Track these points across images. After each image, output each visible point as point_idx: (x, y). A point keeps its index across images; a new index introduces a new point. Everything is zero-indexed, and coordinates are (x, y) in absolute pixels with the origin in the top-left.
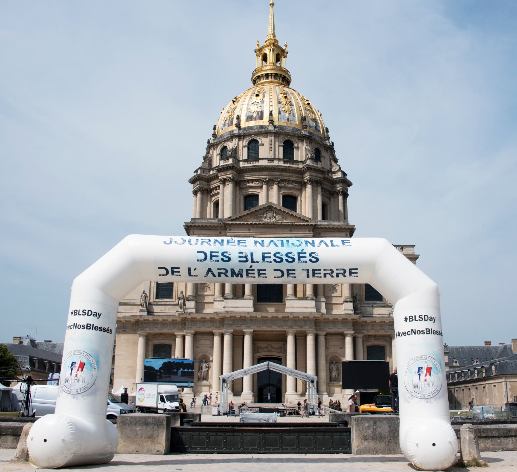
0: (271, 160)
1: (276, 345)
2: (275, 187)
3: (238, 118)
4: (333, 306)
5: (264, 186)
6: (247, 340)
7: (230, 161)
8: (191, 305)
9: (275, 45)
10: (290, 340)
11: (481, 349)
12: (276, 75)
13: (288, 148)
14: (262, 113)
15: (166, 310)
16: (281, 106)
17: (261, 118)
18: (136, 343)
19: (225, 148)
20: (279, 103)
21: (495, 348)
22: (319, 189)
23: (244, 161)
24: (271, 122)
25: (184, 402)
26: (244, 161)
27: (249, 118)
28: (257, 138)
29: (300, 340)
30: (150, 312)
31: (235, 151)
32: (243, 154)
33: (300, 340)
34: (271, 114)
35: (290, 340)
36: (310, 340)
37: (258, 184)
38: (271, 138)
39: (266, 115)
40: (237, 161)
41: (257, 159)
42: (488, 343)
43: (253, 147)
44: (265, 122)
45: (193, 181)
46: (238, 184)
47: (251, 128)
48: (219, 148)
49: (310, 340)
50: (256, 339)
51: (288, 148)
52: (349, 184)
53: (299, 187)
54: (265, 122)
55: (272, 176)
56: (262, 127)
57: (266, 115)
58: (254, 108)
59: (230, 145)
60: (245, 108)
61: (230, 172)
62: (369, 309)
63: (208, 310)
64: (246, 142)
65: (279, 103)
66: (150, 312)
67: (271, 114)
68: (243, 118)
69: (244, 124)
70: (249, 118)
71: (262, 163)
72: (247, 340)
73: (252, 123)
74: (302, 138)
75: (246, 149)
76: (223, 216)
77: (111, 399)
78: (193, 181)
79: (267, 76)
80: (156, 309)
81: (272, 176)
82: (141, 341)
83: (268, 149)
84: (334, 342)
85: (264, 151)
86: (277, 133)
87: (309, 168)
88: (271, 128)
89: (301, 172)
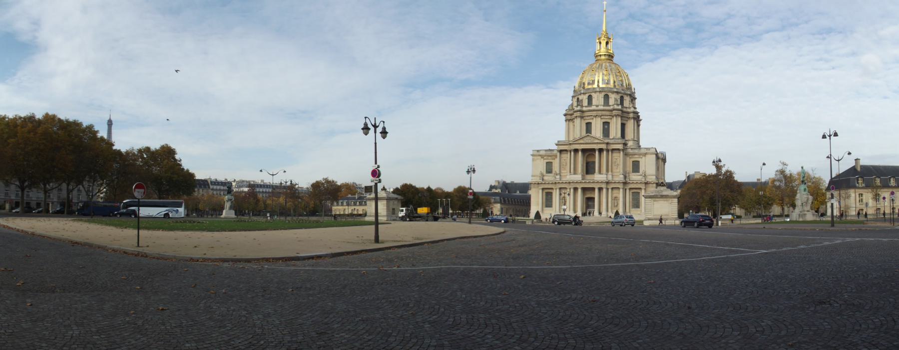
0: (597, 106)
7: (620, 107)
8: (558, 177)
10: (597, 191)
13: (606, 97)
15: (549, 178)
27: (589, 84)
29: (600, 189)
32: (585, 103)
33: (600, 189)
35: (597, 191)
36: (604, 190)
44: (595, 86)
45: (565, 115)
49: (604, 190)
51: (606, 97)
55: (598, 114)
62: (329, 203)
70: (589, 84)
71: (593, 108)
72: (580, 191)
73: (590, 87)
77: (400, 205)
78: (565, 115)
80: (545, 178)
81: (598, 114)
83: (598, 100)
84: (615, 191)
85: (594, 102)
86: (602, 90)
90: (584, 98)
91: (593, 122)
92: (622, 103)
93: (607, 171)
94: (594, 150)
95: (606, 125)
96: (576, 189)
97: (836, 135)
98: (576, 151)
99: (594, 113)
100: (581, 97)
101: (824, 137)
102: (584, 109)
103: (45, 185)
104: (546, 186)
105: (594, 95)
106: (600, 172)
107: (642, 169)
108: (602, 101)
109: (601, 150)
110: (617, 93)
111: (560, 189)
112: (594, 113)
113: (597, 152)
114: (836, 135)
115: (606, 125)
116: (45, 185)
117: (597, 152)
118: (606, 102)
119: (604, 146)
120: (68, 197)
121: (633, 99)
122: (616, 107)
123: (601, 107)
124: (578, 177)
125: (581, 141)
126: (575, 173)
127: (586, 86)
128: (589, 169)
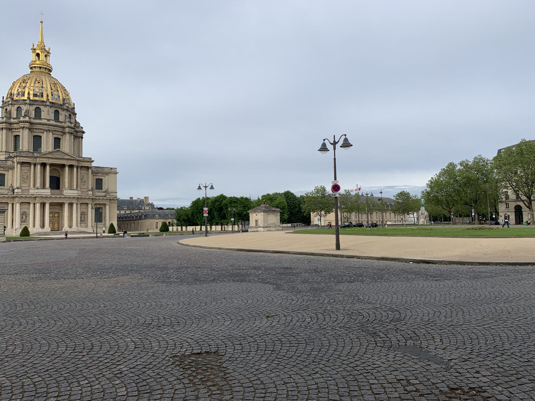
2: (51, 133)
4: (334, 236)
5: (45, 133)
6: (47, 206)
9: (43, 49)
11: (128, 200)
21: (135, 201)
22: (72, 136)
23: (14, 118)
24: (29, 98)
26: (14, 118)
29: (71, 205)
31: (10, 111)
32: (14, 114)
33: (71, 205)
37: (42, 131)
41: (40, 118)
42: (131, 198)
43: (38, 111)
44: (45, 99)
49: (75, 206)
53: (62, 134)
54: (26, 97)
56: (43, 102)
61: (4, 124)
64: (34, 107)
69: (15, 98)
72: (47, 206)
73: (37, 98)
75: (15, 112)
76: (23, 148)
78: (84, 132)
83: (47, 114)
85: (44, 115)
86: (32, 103)
90: (14, 110)
91: (44, 136)
92: (57, 119)
94: (63, 166)
96: (43, 205)
97: (346, 144)
98: (44, 165)
99: (45, 127)
100: (9, 108)
101: (324, 148)
106: (71, 188)
107: (104, 188)
108: (52, 116)
109: (71, 167)
112: (45, 127)
113: (67, 168)
114: (346, 144)
117: (67, 168)
118: (57, 119)
121: (72, 113)
125: (50, 156)
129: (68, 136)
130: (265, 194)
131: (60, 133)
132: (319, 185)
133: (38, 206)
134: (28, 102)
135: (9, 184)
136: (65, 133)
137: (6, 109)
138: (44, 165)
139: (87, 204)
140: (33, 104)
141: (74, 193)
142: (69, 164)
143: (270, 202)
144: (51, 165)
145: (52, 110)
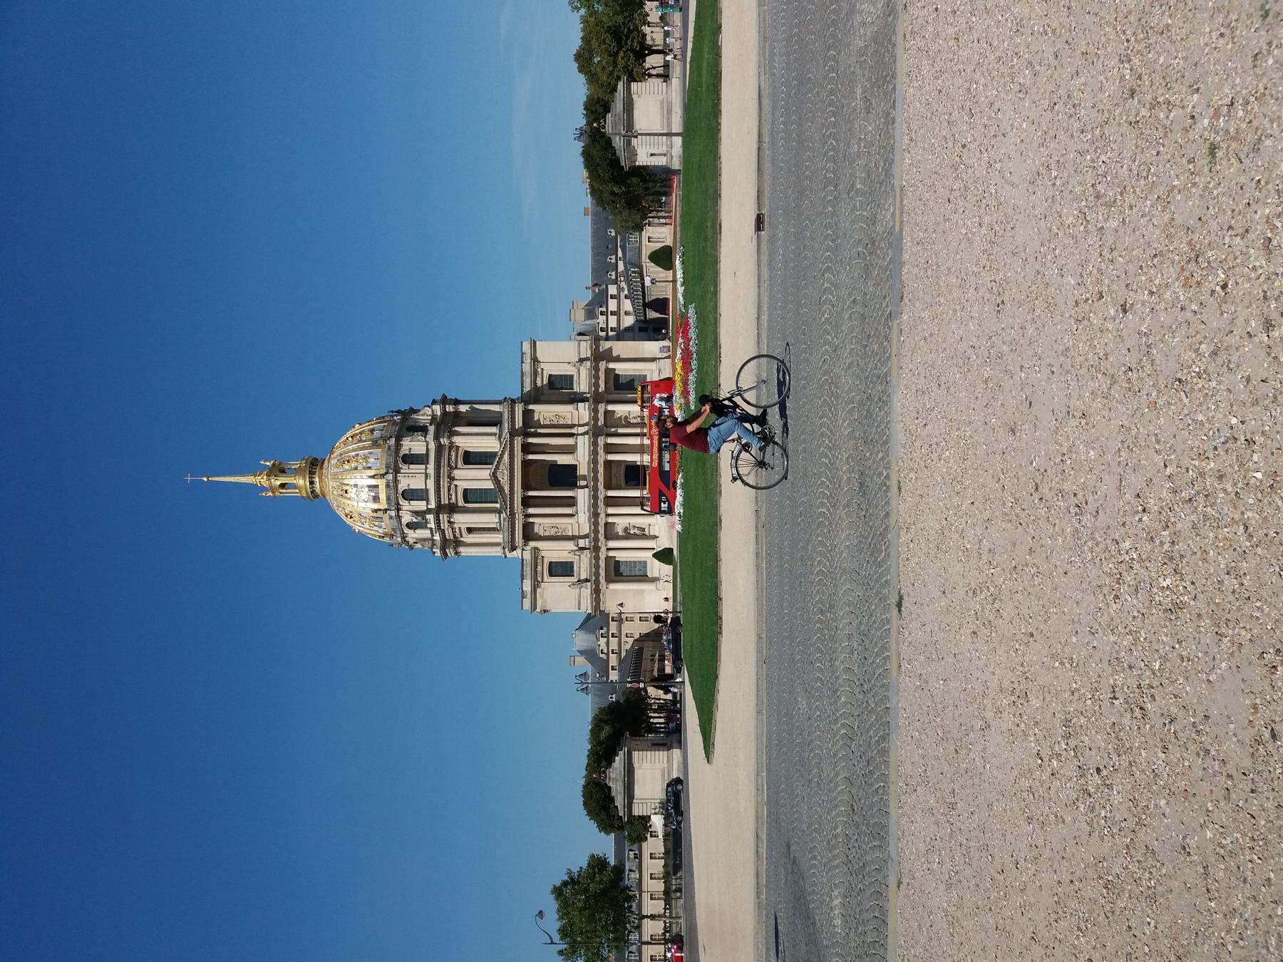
0: (427, 476)
1: (614, 470)
3: (376, 511)
6: (611, 493)
7: (430, 517)
8: (582, 543)
10: (611, 457)
11: (594, 223)
12: (311, 473)
13: (410, 459)
14: (369, 486)
15: (583, 566)
16: (360, 467)
17: (377, 486)
18: (614, 590)
19: (408, 526)
20: (356, 468)
24: (383, 476)
25: (589, 296)
27: (376, 499)
28: (400, 491)
29: (610, 449)
30: (587, 580)
32: (420, 505)
33: (610, 449)
34: (373, 477)
35: (611, 457)
36: (611, 440)
38: (400, 477)
39: (373, 482)
40: (429, 511)
41: (427, 490)
43: (410, 495)
46: (452, 509)
47: (388, 499)
48: (406, 531)
49: (611, 440)
50: (608, 486)
51: (410, 459)
52: (445, 397)
54: (381, 483)
55: (444, 471)
56: (388, 486)
57: (373, 482)
58: (365, 494)
59: (407, 518)
60: (362, 505)
63: (586, 529)
65: (356, 468)
66: (587, 580)
67: (373, 477)
68: (375, 506)
69: (383, 505)
70: (376, 499)
71: (431, 485)
72: (611, 493)
73: (383, 496)
74: (398, 446)
79: (312, 483)
80: (583, 577)
82: (612, 586)
83: (413, 478)
85: (417, 483)
87: (437, 438)
88: (390, 477)
89: (440, 448)
91: (463, 485)
92: (421, 459)
93: (571, 435)
94: (526, 464)
95: (471, 459)
96: (610, 502)
98: (527, 502)
99: (444, 482)
102: (433, 505)
103: (649, 24)
104: (602, 572)
105: (402, 486)
109: (527, 449)
110: (397, 471)
111: (607, 538)
115: (471, 459)
116: (649, 24)
118: (421, 459)
119: (518, 441)
120: (647, 917)
122: (432, 525)
123: (431, 466)
124: (582, 496)
126: (571, 502)
127: (383, 505)
128: (565, 477)
129: (458, 440)
130: (593, 825)
131: (453, 454)
132: (572, 685)
133: (611, 510)
134: (390, 477)
135: (571, 555)
136: (452, 445)
137: (408, 526)
138: (527, 502)
139: (606, 412)
140: (398, 504)
141: (583, 444)
142: (520, 454)
143: (602, 755)
144: (526, 486)
145: (404, 468)
